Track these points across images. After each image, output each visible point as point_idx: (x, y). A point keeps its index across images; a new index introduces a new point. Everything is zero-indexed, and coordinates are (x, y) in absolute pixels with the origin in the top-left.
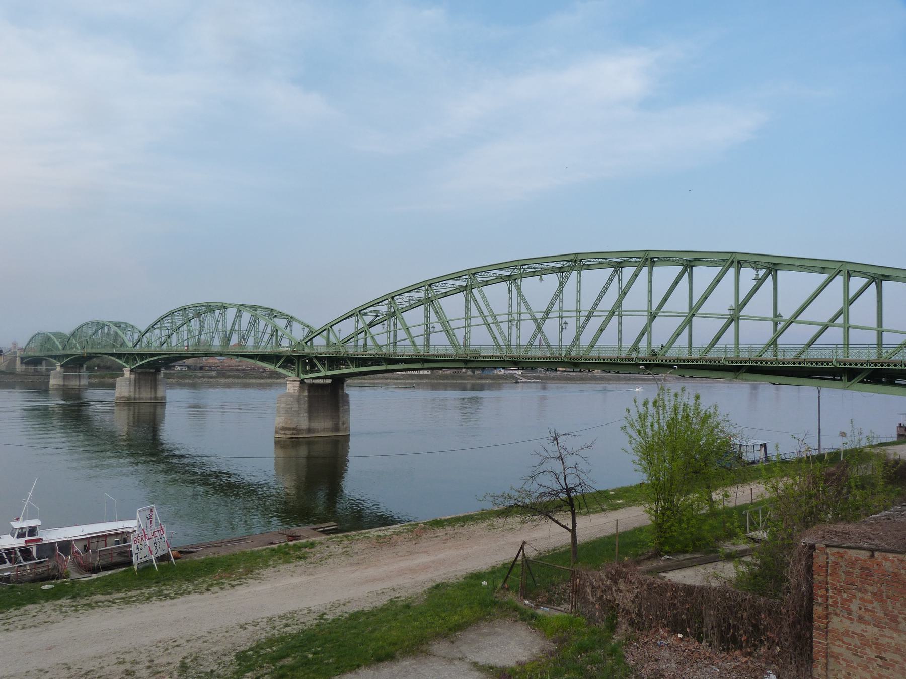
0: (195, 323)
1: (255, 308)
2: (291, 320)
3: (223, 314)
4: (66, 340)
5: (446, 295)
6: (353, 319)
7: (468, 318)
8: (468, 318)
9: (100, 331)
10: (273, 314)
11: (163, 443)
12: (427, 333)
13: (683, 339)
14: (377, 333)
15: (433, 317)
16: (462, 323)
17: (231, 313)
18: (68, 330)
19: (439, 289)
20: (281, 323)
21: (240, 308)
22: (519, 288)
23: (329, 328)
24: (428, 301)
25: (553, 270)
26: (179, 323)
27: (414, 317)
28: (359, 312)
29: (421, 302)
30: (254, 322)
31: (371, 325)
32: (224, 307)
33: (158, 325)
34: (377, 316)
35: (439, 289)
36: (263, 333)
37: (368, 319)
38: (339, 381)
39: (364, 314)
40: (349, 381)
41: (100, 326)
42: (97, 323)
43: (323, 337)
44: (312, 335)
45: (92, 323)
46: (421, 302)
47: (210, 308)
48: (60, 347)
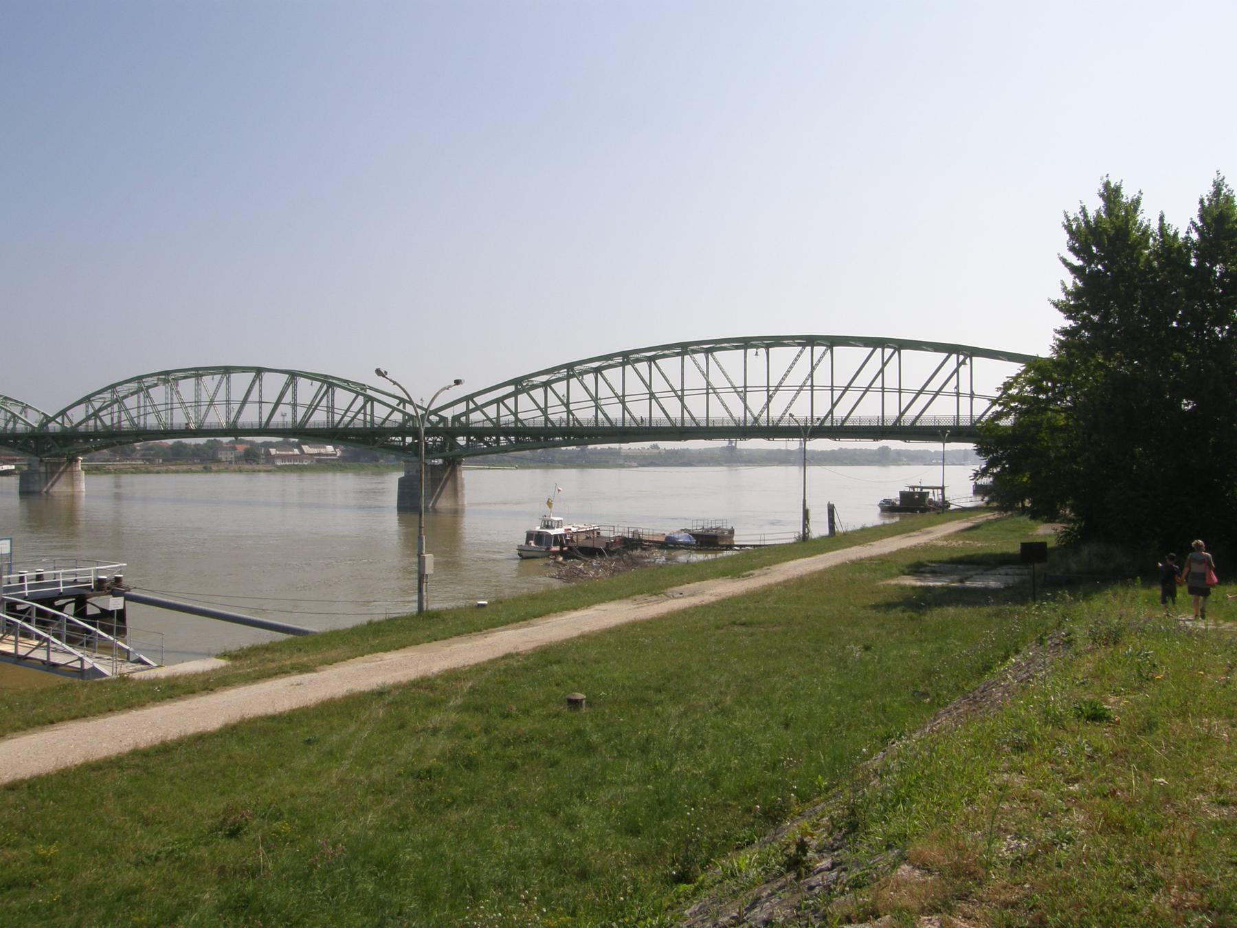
2: (25, 408)
6: (83, 406)
13: (765, 414)
28: (87, 399)
31: (100, 409)
34: (104, 402)
37: (97, 405)
39: (93, 400)
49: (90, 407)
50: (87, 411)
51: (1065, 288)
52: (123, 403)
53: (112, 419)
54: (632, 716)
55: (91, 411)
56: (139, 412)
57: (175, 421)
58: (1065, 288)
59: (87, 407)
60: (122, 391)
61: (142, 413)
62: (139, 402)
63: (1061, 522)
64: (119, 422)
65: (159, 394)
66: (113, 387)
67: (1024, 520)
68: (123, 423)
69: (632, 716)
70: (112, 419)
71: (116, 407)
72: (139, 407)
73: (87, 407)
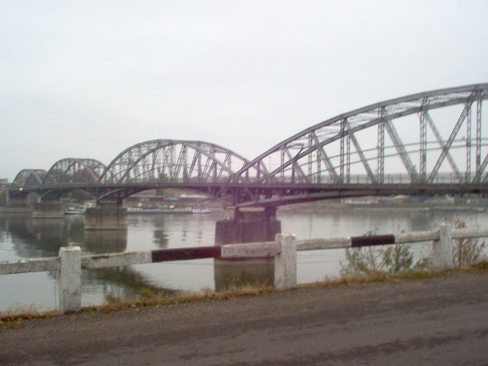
0: (150, 157)
1: (199, 143)
2: (230, 153)
3: (172, 150)
4: (47, 176)
5: (400, 115)
6: (279, 153)
7: (381, 149)
8: (381, 149)
9: (72, 168)
10: (215, 148)
11: (143, 278)
12: (381, 157)
14: (332, 155)
15: (388, 141)
16: (375, 153)
17: (178, 148)
18: (47, 169)
19: (392, 110)
20: (221, 157)
21: (186, 144)
22: (391, 132)
23: (258, 161)
24: (383, 121)
25: (459, 101)
26: (135, 159)
27: (332, 149)
28: (283, 146)
29: (373, 122)
30: (197, 158)
31: (298, 157)
32: (172, 143)
33: (118, 161)
34: (302, 149)
35: (392, 110)
36: (206, 166)
37: (294, 152)
38: (271, 209)
39: (290, 147)
40: (281, 208)
41: (72, 162)
42: (69, 160)
43: (255, 167)
44: (248, 165)
45: (65, 160)
46: (373, 122)
47: (160, 144)
48: (41, 182)
49: (286, 154)
50: (283, 160)
51: (150, 224)
52: (323, 150)
53: (310, 169)
54: (163, 168)
55: (287, 159)
56: (342, 161)
57: (387, 171)
58: (150, 224)
59: (283, 154)
60: (323, 134)
61: (345, 152)
62: (342, 148)
63: (401, 256)
64: (319, 172)
65: (386, 103)
66: (312, 130)
67: (418, 259)
68: (322, 174)
69: (163, 168)
70: (310, 169)
71: (315, 153)
72: (349, 164)
73: (283, 154)
